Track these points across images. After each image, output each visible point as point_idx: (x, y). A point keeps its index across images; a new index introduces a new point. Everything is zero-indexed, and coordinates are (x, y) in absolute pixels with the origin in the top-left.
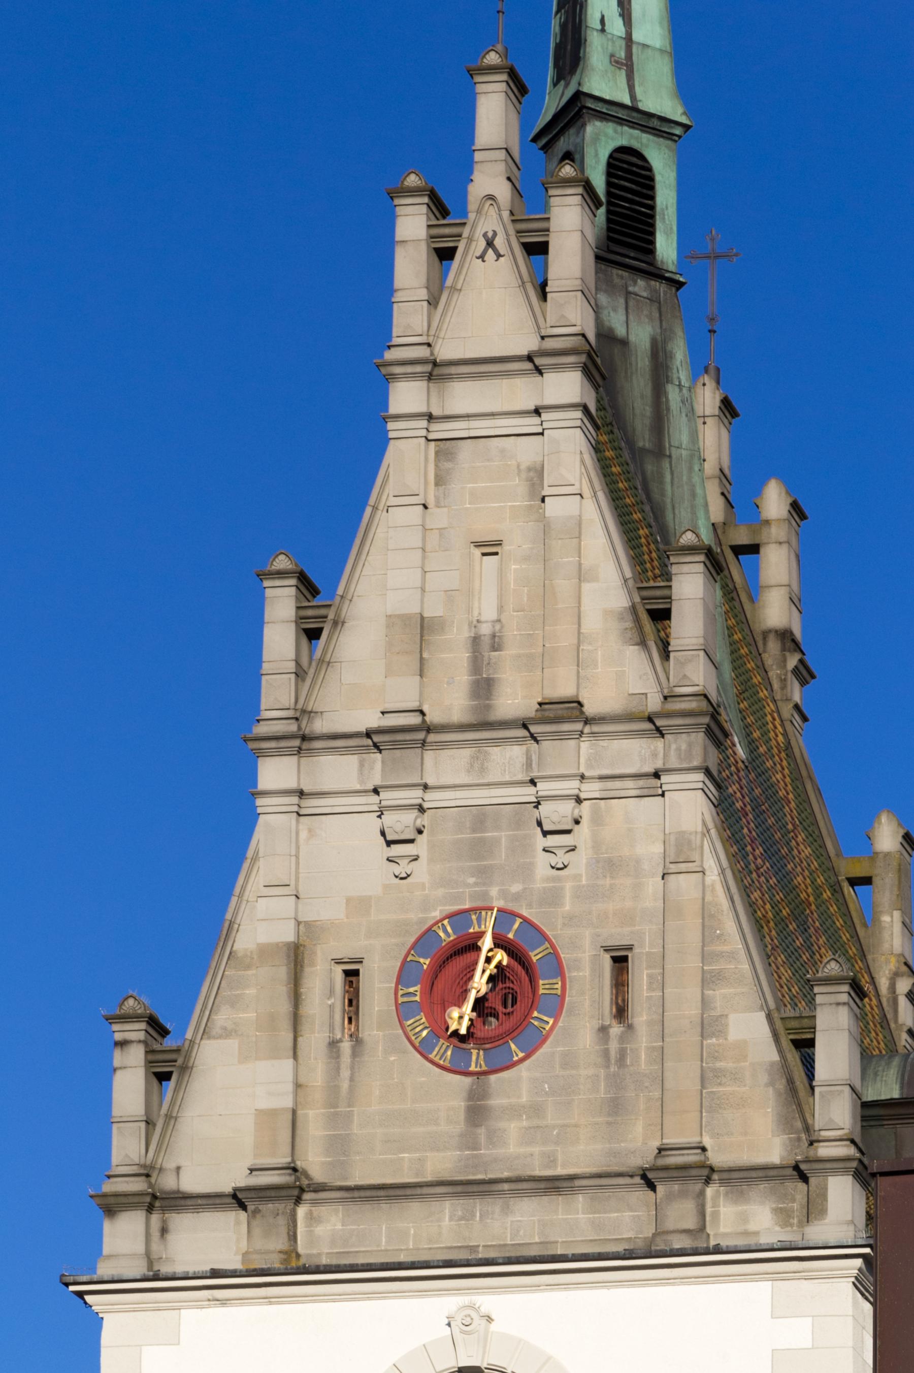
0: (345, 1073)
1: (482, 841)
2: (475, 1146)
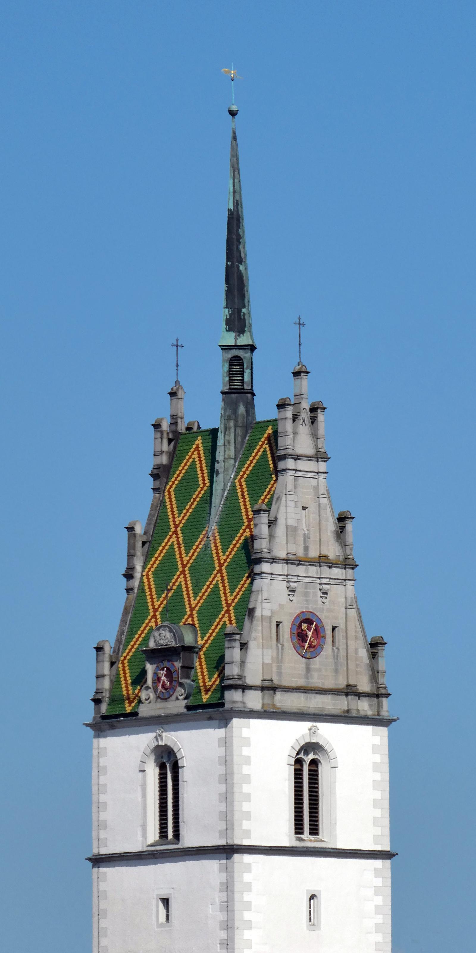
0: (280, 654)
1: (307, 592)
2: (308, 679)
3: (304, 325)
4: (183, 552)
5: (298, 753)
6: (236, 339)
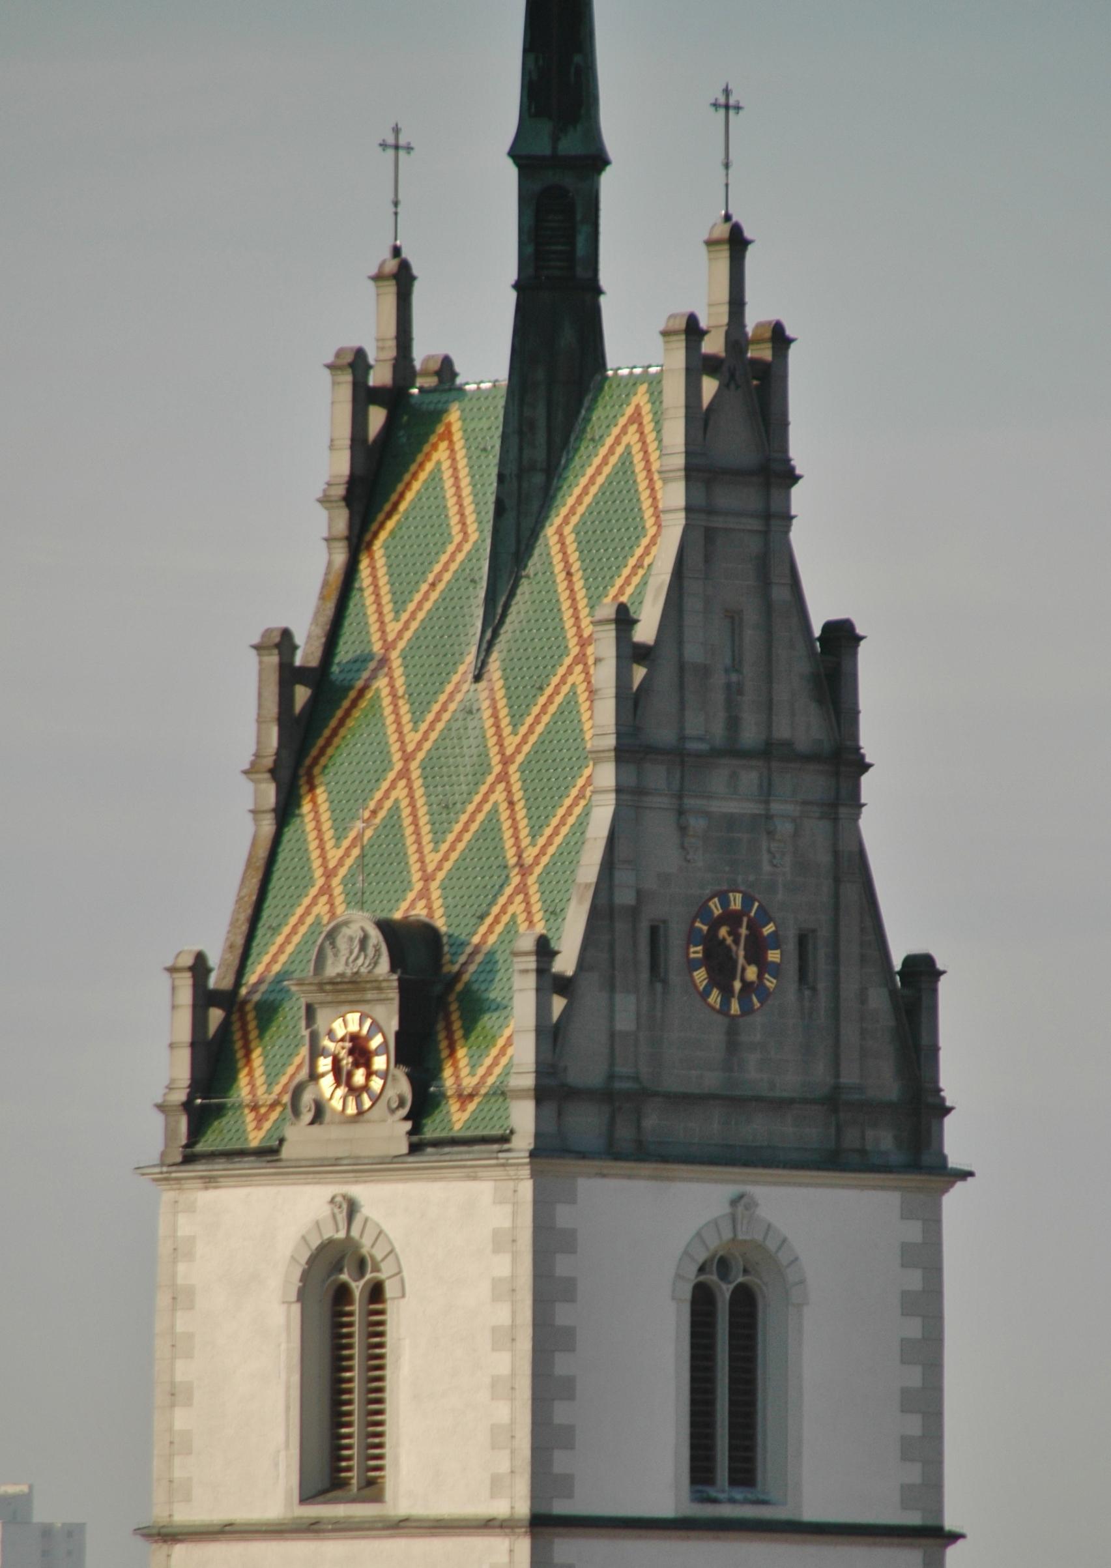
3: (738, 108)
4: (406, 718)
5: (702, 1269)
6: (555, 139)
